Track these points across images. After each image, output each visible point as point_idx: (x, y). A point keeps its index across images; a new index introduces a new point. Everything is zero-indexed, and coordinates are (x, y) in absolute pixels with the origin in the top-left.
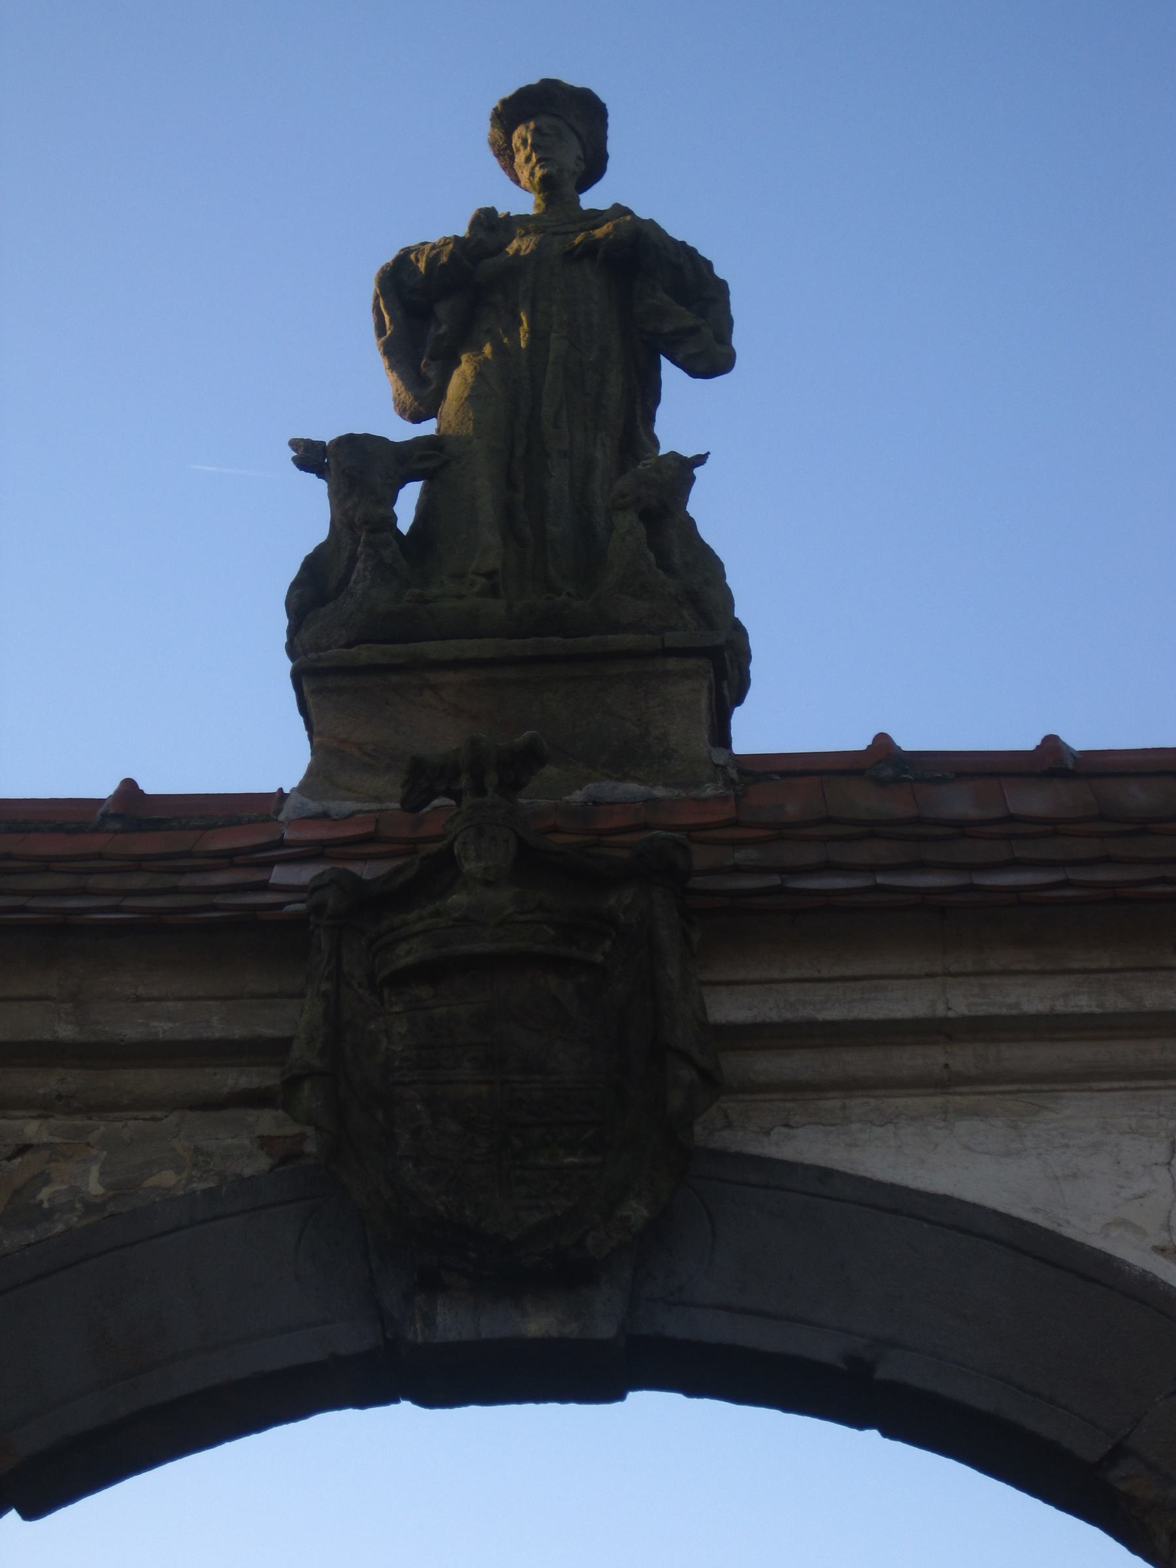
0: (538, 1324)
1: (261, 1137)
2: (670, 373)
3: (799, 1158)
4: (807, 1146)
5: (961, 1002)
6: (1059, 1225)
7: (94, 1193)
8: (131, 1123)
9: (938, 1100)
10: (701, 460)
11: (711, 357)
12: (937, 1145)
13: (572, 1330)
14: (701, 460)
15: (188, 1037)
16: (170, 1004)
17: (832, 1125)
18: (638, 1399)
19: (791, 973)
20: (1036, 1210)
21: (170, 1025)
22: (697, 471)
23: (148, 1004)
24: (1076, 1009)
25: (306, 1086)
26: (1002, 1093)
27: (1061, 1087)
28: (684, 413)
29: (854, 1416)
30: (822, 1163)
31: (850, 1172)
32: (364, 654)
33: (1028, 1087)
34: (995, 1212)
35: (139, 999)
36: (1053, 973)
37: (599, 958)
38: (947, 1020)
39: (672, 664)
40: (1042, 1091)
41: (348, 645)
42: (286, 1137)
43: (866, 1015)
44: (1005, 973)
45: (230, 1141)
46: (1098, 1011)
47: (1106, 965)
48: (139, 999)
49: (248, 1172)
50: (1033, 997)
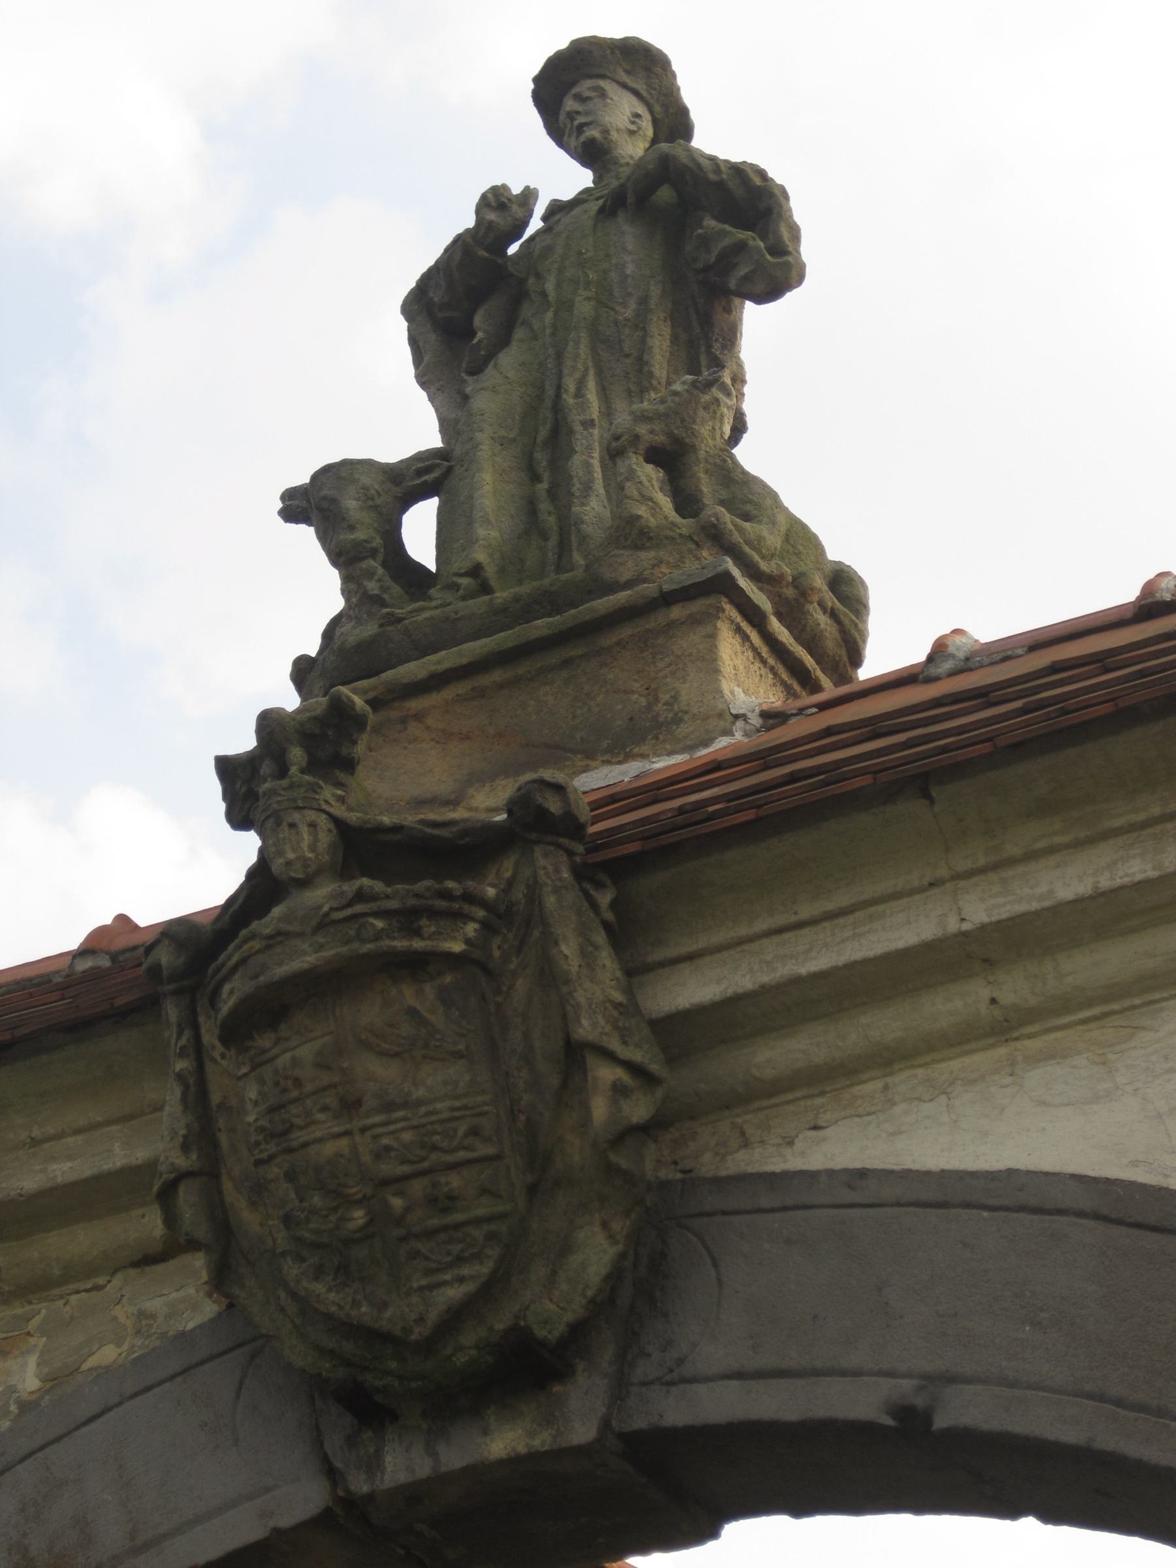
5: (979, 908)
6: (1166, 1176)
8: (74, 1299)
9: (1002, 1051)
12: (1003, 1110)
13: (542, 1441)
16: (70, 1140)
17: (869, 1114)
18: (736, 1532)
19: (761, 925)
20: (1135, 1163)
21: (69, 1164)
23: (47, 1145)
24: (1126, 880)
27: (1157, 996)
31: (896, 1168)
33: (1115, 1006)
34: (1073, 1176)
35: (35, 1143)
36: (1092, 841)
37: (457, 947)
38: (965, 934)
39: (677, 612)
40: (1135, 1007)
43: (859, 955)
44: (1031, 856)
45: (174, 1295)
46: (1153, 874)
47: (1156, 811)
48: (35, 1143)
50: (1067, 881)
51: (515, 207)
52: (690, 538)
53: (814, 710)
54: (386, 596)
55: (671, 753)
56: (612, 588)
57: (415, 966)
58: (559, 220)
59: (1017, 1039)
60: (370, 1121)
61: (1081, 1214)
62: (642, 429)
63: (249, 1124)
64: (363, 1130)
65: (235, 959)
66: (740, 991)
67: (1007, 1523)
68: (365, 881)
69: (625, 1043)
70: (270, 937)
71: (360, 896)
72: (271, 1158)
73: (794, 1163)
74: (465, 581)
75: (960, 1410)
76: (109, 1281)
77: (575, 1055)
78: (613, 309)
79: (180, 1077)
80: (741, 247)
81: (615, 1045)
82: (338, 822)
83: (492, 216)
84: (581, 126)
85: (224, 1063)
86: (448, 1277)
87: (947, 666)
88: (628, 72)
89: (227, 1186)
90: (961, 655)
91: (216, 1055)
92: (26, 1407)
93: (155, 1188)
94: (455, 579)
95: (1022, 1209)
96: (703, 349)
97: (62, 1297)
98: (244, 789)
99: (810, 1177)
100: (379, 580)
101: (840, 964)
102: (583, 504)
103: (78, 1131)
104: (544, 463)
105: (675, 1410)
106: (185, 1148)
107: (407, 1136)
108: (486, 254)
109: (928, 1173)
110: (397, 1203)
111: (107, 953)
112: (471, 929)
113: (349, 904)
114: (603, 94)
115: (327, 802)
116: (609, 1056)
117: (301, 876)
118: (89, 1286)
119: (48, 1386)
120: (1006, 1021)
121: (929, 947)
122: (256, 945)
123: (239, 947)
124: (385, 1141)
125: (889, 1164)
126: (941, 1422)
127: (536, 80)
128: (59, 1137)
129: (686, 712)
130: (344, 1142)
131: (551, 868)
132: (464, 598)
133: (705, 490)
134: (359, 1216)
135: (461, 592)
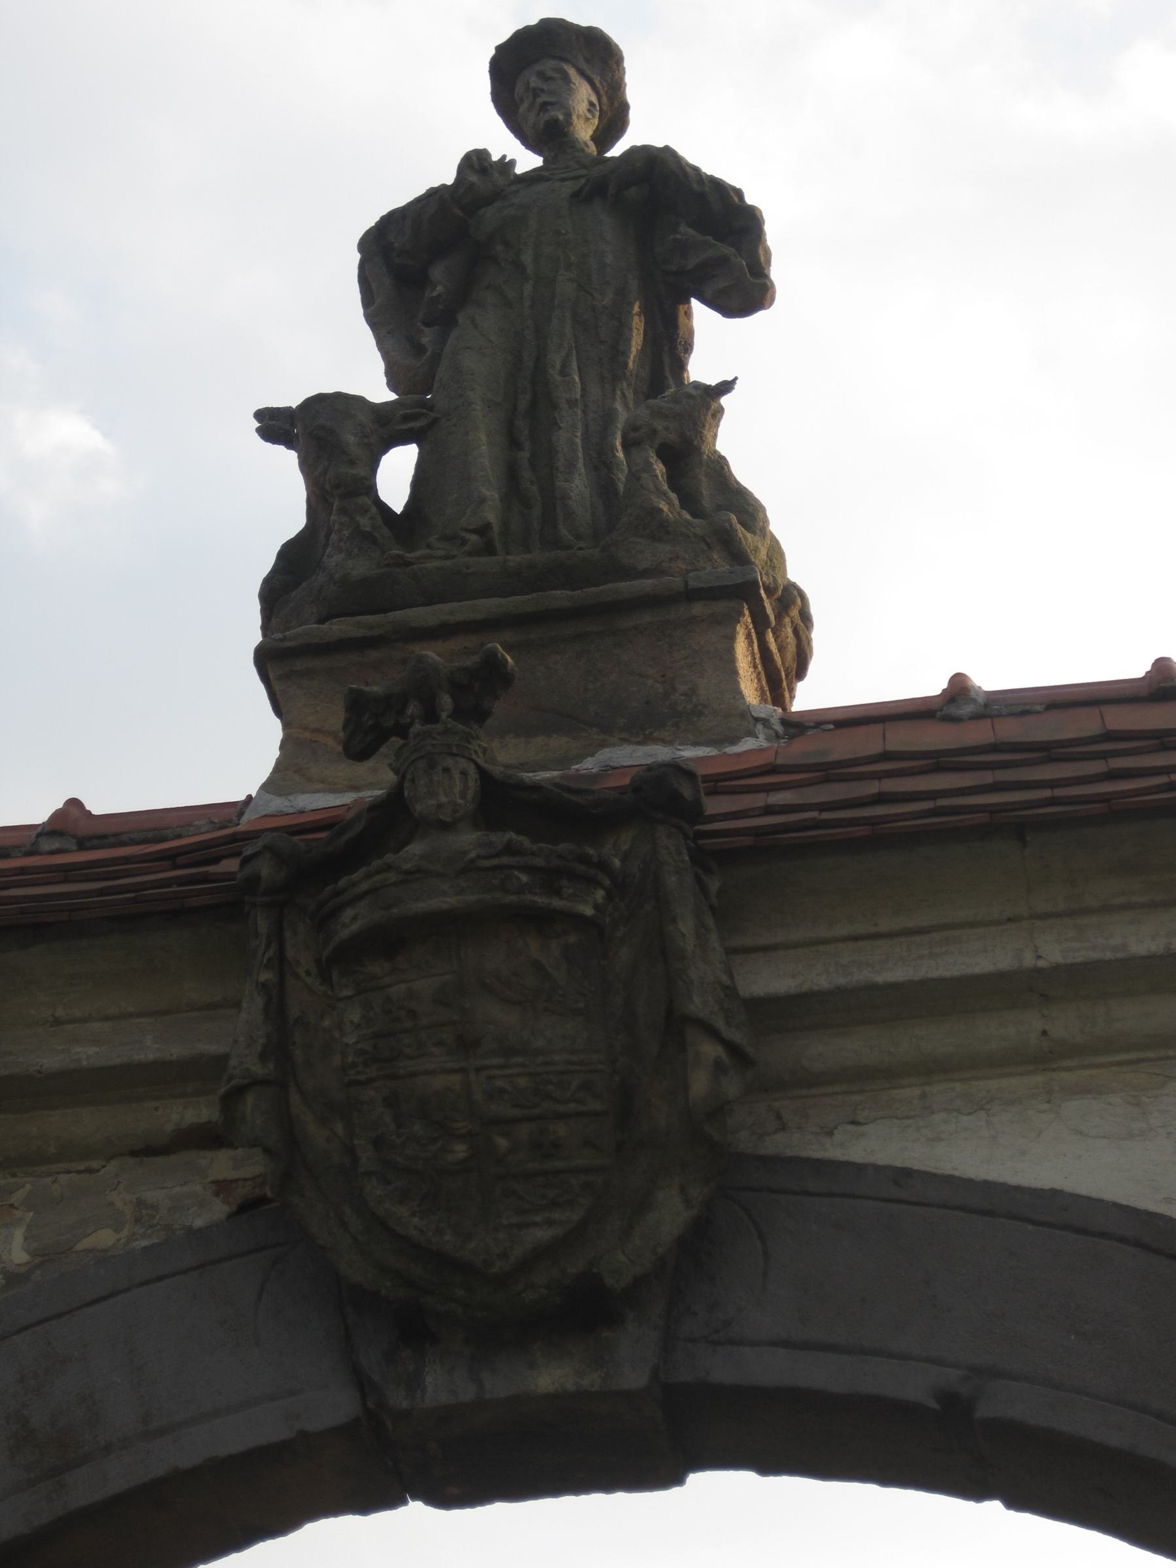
0: (551, 1377)
1: (216, 1182)
2: (702, 316)
3: (871, 1159)
4: (881, 1143)
5: (1054, 949)
7: (17, 1261)
8: (63, 1178)
9: (1039, 1079)
10: (726, 387)
11: (745, 291)
13: (592, 1381)
14: (726, 387)
15: (118, 1061)
17: (908, 1118)
18: (698, 1480)
19: (841, 930)
22: (725, 401)
23: (70, 1027)
25: (250, 1099)
26: (1120, 1064)
28: (714, 343)
29: (970, 1484)
30: (898, 1163)
32: (340, 628)
34: (1115, 1205)
35: (57, 1022)
37: (588, 911)
38: (1038, 971)
39: (698, 609)
41: (321, 621)
42: (245, 1180)
43: (935, 974)
44: (1106, 909)
45: (178, 1189)
48: (57, 1022)
49: (199, 1223)
51: (496, 175)
52: (703, 539)
53: (832, 727)
54: (376, 534)
55: (696, 744)
56: (630, 573)
57: (541, 921)
58: (517, 191)
59: (1054, 1070)
60: (487, 1062)
61: (1122, 1240)
62: (659, 425)
63: (347, 1045)
64: (478, 1070)
65: (364, 886)
66: (816, 988)
67: (971, 1505)
68: (511, 835)
69: (728, 1024)
70: (409, 872)
71: (509, 849)
72: (370, 1081)
73: (833, 1152)
74: (474, 538)
75: (1003, 1403)
76: (104, 1166)
77: (676, 1026)
78: (591, 295)
79: (264, 987)
80: (723, 261)
81: (720, 1024)
82: (481, 770)
83: (473, 178)
84: (544, 106)
85: (309, 980)
86: (538, 1219)
87: (967, 710)
88: (587, 60)
89: (295, 1098)
90: (981, 700)
91: (301, 971)
92: (14, 1278)
93: (223, 1090)
94: (464, 534)
95: (1065, 1227)
96: (666, 348)
97: (50, 1174)
98: (371, 722)
99: (859, 1169)
100: (372, 518)
101: (916, 979)
102: (566, 481)
103: (107, 1018)
104: (526, 432)
105: (722, 1369)
106: (263, 1057)
107: (522, 1082)
108: (461, 214)
109: (970, 1182)
110: (502, 1143)
111: (74, 837)
112: (600, 894)
113: (497, 855)
114: (566, 78)
115: (476, 752)
116: (713, 1033)
117: (448, 820)
118: (83, 1168)
119: (37, 1261)
120: (1051, 1052)
121: (1001, 976)
122: (392, 877)
123: (369, 876)
124: (499, 1083)
125: (929, 1166)
126: (984, 1411)
127: (500, 49)
128: (83, 1020)
129: (706, 707)
130: (456, 1079)
131: (670, 847)
132: (470, 554)
133: (705, 493)
134: (460, 1150)
135: (467, 548)
